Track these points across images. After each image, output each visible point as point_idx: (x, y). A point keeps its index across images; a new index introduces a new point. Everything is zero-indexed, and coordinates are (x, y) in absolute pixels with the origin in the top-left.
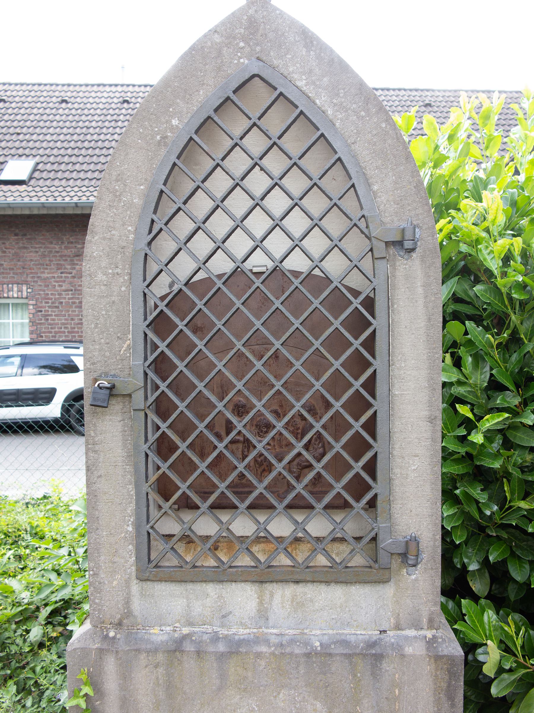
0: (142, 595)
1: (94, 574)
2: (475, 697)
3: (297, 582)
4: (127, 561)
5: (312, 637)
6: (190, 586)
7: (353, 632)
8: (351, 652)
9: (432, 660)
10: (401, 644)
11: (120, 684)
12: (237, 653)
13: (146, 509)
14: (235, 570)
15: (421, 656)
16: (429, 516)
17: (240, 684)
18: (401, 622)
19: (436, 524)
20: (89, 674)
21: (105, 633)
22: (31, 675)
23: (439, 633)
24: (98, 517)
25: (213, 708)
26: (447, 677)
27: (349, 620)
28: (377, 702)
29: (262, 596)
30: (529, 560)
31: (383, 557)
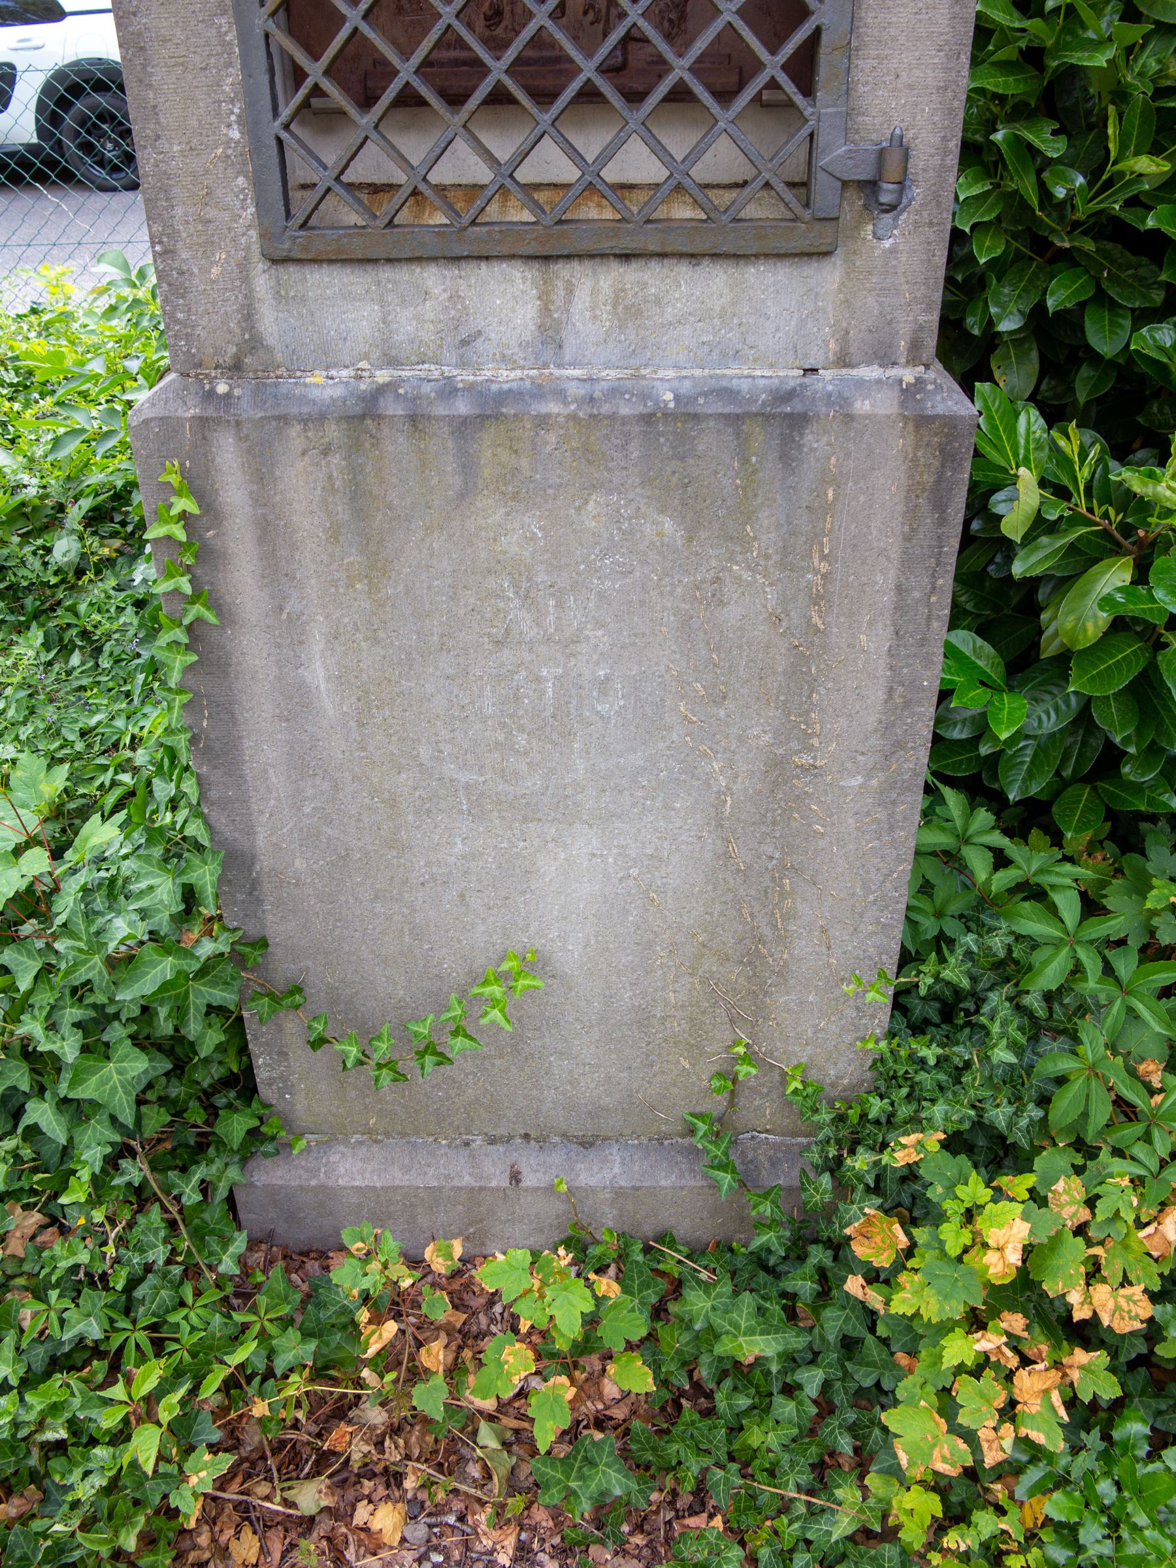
0: (280, 297)
1: (166, 252)
2: (975, 606)
3: (626, 257)
4: (236, 218)
5: (658, 383)
6: (386, 273)
7: (746, 372)
8: (739, 411)
9: (911, 427)
10: (847, 394)
11: (251, 492)
12: (497, 417)
13: (266, 78)
14: (484, 229)
15: (888, 417)
16: (938, 88)
17: (505, 484)
18: (852, 350)
19: (951, 111)
20: (183, 472)
21: (207, 387)
22: (72, 620)
23: (931, 375)
24: (155, 107)
25: (451, 536)
26: (936, 463)
27: (740, 346)
28: (788, 516)
29: (548, 293)
30: (1133, 310)
31: (825, 193)
